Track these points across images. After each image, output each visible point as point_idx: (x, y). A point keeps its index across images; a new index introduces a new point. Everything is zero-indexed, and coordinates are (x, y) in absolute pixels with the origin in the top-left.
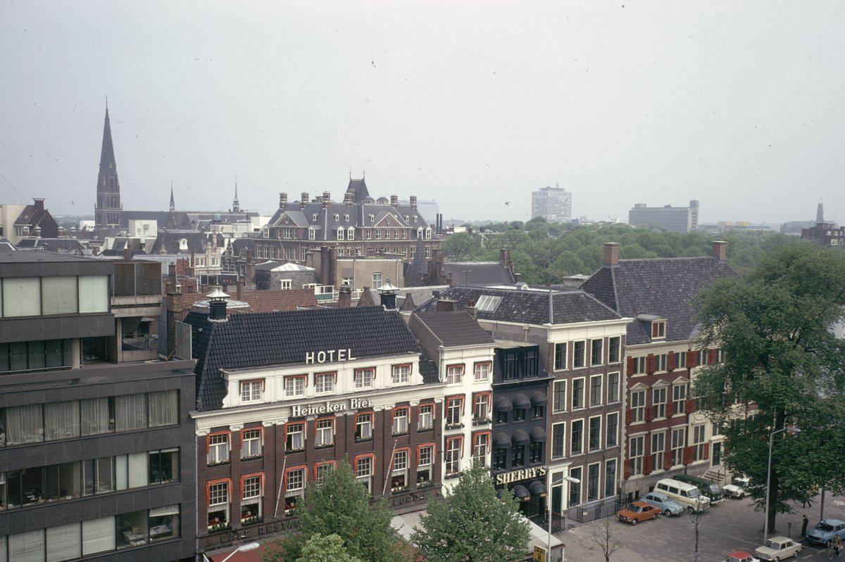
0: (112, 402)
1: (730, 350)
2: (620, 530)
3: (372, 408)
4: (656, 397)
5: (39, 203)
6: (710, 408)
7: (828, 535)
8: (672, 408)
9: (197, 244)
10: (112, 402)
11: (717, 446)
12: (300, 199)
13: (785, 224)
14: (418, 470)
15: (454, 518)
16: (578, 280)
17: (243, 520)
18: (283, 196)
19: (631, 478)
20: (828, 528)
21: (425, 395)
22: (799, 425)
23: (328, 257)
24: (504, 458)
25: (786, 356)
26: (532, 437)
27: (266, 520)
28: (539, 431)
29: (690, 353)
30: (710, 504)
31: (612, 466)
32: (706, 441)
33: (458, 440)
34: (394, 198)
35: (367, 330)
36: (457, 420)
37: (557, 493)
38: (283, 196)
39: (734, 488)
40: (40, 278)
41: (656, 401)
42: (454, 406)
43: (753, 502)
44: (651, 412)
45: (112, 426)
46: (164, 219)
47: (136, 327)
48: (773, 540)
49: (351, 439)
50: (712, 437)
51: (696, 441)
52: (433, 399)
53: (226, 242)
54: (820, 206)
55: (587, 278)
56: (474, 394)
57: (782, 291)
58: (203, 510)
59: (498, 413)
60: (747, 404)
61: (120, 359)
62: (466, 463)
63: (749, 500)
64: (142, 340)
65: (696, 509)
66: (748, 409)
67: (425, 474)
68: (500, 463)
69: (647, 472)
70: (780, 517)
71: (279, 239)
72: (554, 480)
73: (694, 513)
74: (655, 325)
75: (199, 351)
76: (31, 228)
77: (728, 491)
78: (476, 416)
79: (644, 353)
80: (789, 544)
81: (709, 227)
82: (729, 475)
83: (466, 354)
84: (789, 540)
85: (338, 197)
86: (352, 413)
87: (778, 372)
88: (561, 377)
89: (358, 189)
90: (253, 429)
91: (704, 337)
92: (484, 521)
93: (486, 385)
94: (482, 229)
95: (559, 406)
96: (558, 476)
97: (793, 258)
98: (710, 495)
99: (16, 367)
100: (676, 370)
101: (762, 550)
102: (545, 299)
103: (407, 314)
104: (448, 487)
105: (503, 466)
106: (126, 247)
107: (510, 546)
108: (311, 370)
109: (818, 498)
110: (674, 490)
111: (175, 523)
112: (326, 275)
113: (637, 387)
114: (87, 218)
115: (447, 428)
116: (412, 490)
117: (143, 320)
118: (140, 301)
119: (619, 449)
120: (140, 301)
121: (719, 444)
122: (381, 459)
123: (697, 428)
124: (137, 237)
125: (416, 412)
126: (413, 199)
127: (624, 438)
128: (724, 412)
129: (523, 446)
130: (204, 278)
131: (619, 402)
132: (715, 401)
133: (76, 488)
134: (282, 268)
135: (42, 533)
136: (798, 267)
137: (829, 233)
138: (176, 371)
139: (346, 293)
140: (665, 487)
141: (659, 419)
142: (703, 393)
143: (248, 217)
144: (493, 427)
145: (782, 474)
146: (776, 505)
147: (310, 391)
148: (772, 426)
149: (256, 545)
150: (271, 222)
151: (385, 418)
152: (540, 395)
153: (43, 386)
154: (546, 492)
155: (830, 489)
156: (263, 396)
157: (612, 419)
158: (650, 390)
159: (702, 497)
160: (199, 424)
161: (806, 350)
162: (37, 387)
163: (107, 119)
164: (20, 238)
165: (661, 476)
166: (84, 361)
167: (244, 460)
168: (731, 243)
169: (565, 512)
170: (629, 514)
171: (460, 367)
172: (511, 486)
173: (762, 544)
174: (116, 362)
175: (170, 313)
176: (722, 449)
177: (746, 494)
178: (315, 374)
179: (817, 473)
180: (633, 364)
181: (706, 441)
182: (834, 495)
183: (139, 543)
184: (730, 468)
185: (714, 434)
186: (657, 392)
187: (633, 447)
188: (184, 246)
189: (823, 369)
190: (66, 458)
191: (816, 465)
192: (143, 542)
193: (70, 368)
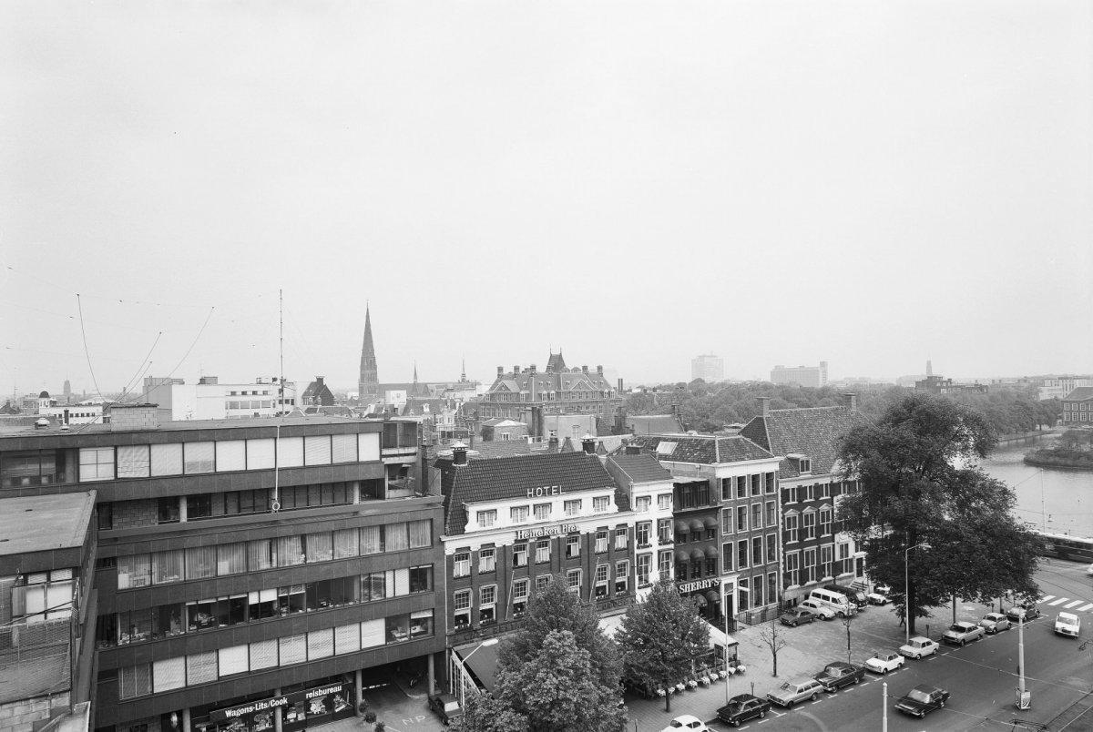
0: (382, 529)
1: (866, 480)
2: (784, 632)
3: (579, 532)
4: (807, 521)
5: (320, 380)
6: (852, 529)
7: (960, 636)
8: (820, 530)
9: (436, 407)
10: (382, 529)
11: (860, 561)
12: (513, 371)
13: (900, 378)
14: (617, 581)
15: (649, 621)
16: (735, 427)
17: (481, 622)
18: (500, 369)
19: (789, 588)
20: (961, 630)
21: (621, 521)
22: (929, 541)
23: (537, 413)
24: (685, 573)
25: (915, 485)
26: (706, 554)
27: (499, 622)
28: (713, 550)
29: (832, 485)
30: (858, 610)
31: (773, 578)
32: (850, 557)
33: (647, 558)
34: (585, 368)
35: (571, 470)
36: (646, 541)
37: (730, 598)
38: (500, 369)
39: (877, 596)
40: (149, 445)
41: (807, 524)
42: (643, 530)
43: (894, 608)
44: (803, 533)
45: (383, 546)
46: (413, 388)
47: (398, 471)
48: (915, 640)
49: (563, 556)
50: (854, 554)
51: (842, 556)
52: (469, 548)
53: (458, 404)
54: (929, 363)
55: (743, 426)
56: (659, 520)
57: (907, 431)
58: (450, 614)
59: (678, 534)
60: (883, 526)
61: (387, 496)
62: (654, 576)
63: (891, 606)
64: (403, 481)
65: (846, 613)
66: (884, 529)
67: (622, 585)
68: (682, 575)
69: (802, 583)
70: (919, 620)
71: (499, 401)
72: (726, 590)
73: (845, 617)
74: (802, 462)
75: (446, 491)
76: (314, 399)
77: (871, 598)
78: (661, 538)
79: (794, 485)
80: (929, 644)
81: (837, 382)
82: (872, 585)
83: (651, 488)
84: (927, 640)
85: (542, 368)
86: (564, 536)
87: (909, 499)
88: (730, 503)
89: (556, 363)
90: (487, 550)
91: (844, 471)
92: (672, 623)
93: (669, 514)
94: (654, 390)
95: (726, 529)
96: (729, 586)
97: (914, 404)
98: (857, 601)
99: (314, 503)
100: (821, 499)
101: (906, 648)
102: (712, 444)
103: (603, 458)
104: (642, 595)
105: (685, 578)
106: (384, 411)
107: (695, 643)
108: (531, 502)
109: (950, 604)
110: (826, 598)
111: (430, 623)
112: (536, 429)
113: (790, 513)
114: (353, 390)
115: (638, 548)
116: (613, 598)
117: (403, 466)
118: (402, 451)
119: (778, 563)
120: (402, 451)
121: (861, 559)
122: (587, 571)
123: (842, 546)
124: (392, 402)
125: (615, 534)
126: (600, 368)
127: (782, 555)
128: (864, 532)
129: (700, 562)
130: (443, 433)
131: (776, 525)
132: (855, 523)
133: (356, 596)
134: (502, 424)
135: (331, 631)
136: (919, 413)
137: (938, 385)
138: (429, 505)
139: (554, 442)
140: (818, 596)
141: (810, 539)
142: (846, 517)
143: (474, 386)
144: (675, 546)
145: (919, 583)
146: (915, 611)
147: (531, 519)
148: (905, 543)
149: (494, 641)
150: (491, 389)
151: (589, 540)
152: (713, 522)
153: (332, 518)
154: (720, 600)
155: (960, 596)
156: (496, 524)
157: (771, 539)
158: (801, 515)
159: (850, 604)
160: (447, 545)
161: (931, 480)
162: (328, 518)
163: (368, 316)
164: (306, 407)
165: (814, 586)
166: (362, 499)
167: (482, 573)
168: (858, 395)
169: (736, 616)
170: (790, 619)
171: (647, 498)
172: (693, 593)
173: (904, 643)
174: (384, 498)
175: (424, 460)
176: (864, 563)
177: (888, 601)
178: (534, 505)
179: (948, 581)
180: (785, 493)
181: (850, 557)
182: (964, 601)
183: (403, 639)
184: (872, 580)
185: (857, 551)
186: (807, 516)
187: (790, 562)
188: (426, 410)
189: (946, 495)
190: (350, 572)
191: (947, 575)
192: (406, 639)
193: (179, 521)
